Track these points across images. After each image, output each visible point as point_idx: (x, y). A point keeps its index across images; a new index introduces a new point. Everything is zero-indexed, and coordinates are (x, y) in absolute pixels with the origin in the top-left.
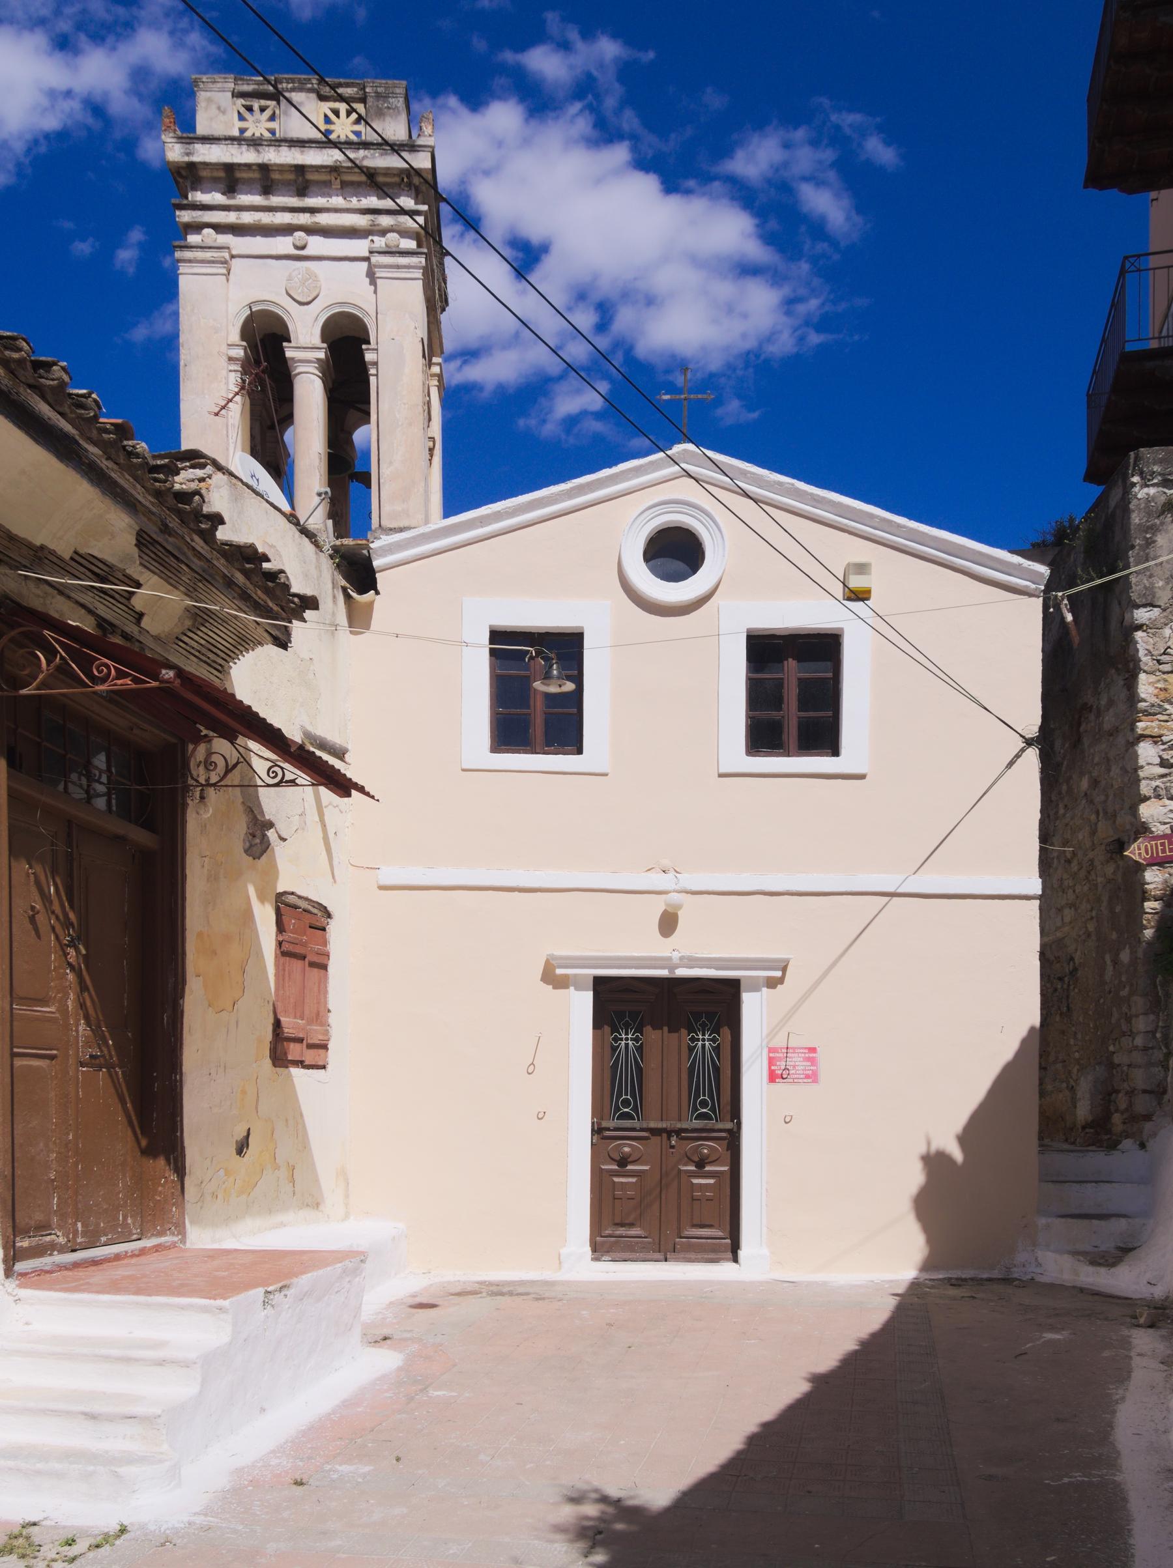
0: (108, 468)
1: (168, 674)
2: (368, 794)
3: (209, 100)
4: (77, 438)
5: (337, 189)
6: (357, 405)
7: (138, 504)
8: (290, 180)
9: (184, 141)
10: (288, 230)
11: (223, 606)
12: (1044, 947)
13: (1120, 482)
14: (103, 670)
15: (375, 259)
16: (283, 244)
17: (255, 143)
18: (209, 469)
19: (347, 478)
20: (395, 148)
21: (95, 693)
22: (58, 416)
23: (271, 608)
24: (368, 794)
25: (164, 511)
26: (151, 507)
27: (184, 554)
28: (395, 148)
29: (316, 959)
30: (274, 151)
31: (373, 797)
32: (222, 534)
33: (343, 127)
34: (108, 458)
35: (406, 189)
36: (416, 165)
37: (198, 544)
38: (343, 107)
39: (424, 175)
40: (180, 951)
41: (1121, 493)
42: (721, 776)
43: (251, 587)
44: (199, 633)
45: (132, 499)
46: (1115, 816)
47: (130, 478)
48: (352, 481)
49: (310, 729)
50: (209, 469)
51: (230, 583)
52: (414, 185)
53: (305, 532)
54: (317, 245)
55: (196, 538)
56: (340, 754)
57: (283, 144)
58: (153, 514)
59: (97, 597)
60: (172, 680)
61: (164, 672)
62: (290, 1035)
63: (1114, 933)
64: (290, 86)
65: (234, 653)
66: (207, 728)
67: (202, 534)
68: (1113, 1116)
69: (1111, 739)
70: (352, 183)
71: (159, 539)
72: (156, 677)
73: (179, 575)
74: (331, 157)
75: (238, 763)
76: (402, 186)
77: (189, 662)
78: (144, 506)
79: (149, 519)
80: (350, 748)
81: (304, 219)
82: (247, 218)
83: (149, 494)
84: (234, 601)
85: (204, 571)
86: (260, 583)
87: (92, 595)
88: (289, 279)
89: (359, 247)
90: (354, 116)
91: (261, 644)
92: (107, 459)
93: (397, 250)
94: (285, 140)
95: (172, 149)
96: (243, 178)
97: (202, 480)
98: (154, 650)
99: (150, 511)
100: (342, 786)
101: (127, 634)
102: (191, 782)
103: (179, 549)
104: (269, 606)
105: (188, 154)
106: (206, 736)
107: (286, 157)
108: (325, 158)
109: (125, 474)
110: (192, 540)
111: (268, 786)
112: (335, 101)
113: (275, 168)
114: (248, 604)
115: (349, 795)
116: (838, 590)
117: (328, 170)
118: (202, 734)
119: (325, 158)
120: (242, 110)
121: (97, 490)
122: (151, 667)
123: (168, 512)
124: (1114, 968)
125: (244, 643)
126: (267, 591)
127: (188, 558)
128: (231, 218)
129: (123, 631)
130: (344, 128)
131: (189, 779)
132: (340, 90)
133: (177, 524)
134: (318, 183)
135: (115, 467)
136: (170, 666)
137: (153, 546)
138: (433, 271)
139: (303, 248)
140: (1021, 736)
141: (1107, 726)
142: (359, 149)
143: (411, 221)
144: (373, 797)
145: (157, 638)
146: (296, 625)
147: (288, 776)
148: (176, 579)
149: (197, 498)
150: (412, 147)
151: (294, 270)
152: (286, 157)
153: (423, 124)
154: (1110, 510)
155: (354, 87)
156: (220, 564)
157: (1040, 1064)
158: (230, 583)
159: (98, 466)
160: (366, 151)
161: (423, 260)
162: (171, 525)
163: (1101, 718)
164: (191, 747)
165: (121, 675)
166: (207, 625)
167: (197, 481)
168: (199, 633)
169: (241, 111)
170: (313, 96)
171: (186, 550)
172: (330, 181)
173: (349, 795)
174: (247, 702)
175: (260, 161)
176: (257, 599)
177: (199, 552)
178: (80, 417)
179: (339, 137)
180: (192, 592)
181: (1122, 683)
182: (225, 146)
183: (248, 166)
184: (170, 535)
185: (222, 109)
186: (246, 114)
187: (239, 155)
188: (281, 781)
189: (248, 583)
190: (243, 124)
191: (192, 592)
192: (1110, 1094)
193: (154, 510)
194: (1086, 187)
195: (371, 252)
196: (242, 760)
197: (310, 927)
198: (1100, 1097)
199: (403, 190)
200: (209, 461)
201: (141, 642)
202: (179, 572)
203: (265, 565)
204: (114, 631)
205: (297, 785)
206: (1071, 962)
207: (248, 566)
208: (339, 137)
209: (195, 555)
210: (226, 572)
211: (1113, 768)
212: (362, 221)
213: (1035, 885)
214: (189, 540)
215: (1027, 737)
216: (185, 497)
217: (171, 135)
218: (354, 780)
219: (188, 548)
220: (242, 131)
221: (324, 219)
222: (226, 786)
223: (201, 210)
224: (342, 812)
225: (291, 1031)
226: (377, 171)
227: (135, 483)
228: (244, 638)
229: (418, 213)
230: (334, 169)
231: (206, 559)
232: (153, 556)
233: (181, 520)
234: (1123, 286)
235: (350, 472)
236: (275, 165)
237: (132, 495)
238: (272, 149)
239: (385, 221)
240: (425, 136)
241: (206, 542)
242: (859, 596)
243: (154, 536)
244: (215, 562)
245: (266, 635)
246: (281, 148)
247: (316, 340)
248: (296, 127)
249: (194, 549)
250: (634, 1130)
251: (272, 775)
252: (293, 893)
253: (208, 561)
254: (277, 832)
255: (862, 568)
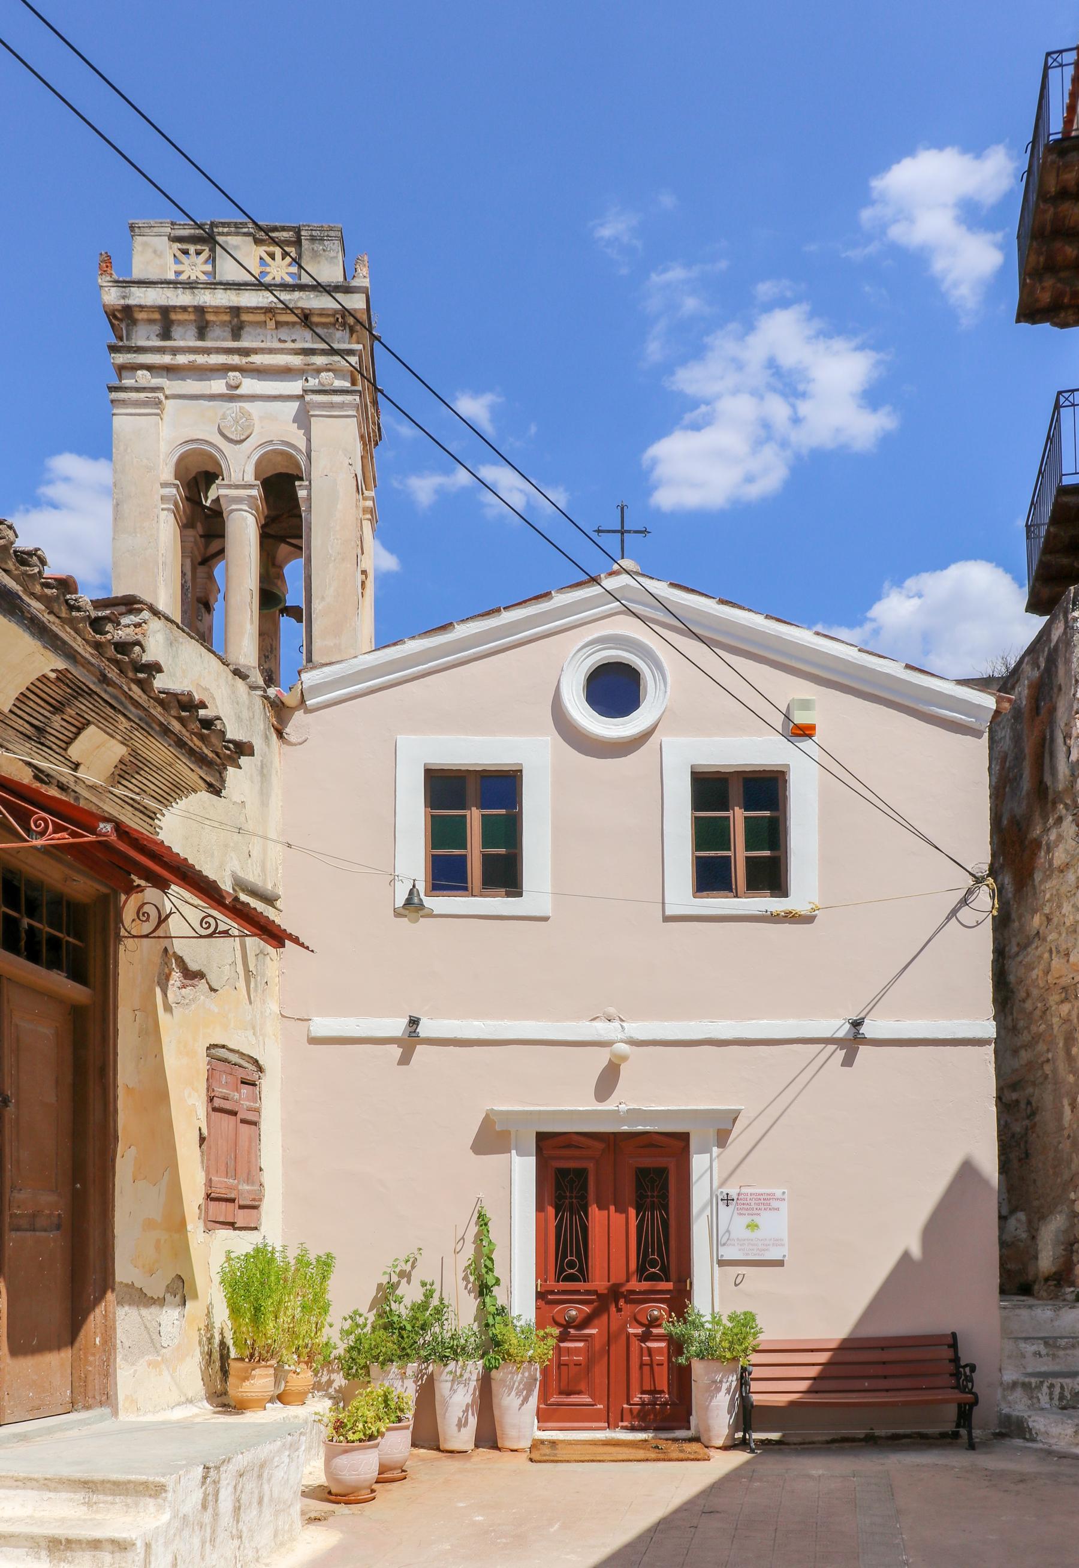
0: (49, 622)
1: (106, 828)
2: (302, 945)
3: (145, 245)
4: (21, 593)
5: (271, 329)
6: (288, 540)
7: (79, 656)
8: (225, 321)
9: (120, 285)
10: (224, 370)
11: (158, 751)
12: (1000, 1090)
13: (1061, 617)
14: (40, 824)
15: (308, 398)
16: (218, 386)
17: (191, 285)
18: (146, 614)
19: (278, 611)
20: (329, 290)
21: (34, 848)
22: (3, 573)
23: (206, 755)
24: (302, 945)
25: (103, 662)
26: (91, 658)
27: (121, 703)
28: (329, 290)
29: (250, 1116)
30: (210, 294)
31: (307, 948)
32: (160, 682)
33: (279, 269)
34: (51, 612)
35: (341, 328)
36: (348, 306)
37: (136, 692)
38: (278, 251)
39: (358, 315)
40: (111, 1109)
41: (1063, 627)
42: (667, 919)
43: (187, 734)
44: (133, 781)
45: (73, 652)
46: (1067, 955)
47: (71, 631)
48: (283, 616)
49: (241, 874)
50: (146, 614)
51: (166, 731)
52: (349, 324)
53: (237, 673)
54: (250, 385)
55: (134, 687)
56: (270, 900)
57: (219, 287)
58: (92, 665)
59: (34, 749)
60: (109, 834)
61: (102, 825)
62: (222, 1195)
63: (1071, 1076)
64: (226, 230)
65: (168, 800)
66: (140, 878)
67: (139, 683)
68: (1076, 1268)
69: (1062, 875)
70: (287, 323)
71: (98, 690)
72: (93, 831)
73: (116, 724)
74: (263, 299)
75: (171, 913)
76: (337, 326)
77: (124, 811)
78: (82, 657)
79: (88, 671)
80: (280, 891)
81: (235, 360)
82: (182, 359)
83: (90, 646)
84: (169, 748)
85: (140, 720)
86: (195, 730)
87: (30, 746)
88: (224, 417)
89: (295, 387)
90: (288, 259)
91: (195, 791)
92: (49, 613)
93: (332, 388)
94: (221, 283)
95: (109, 293)
96: (179, 320)
97: (138, 625)
98: (89, 800)
99: (89, 663)
100: (275, 936)
101: (63, 784)
102: (123, 933)
103: (115, 698)
104: (204, 753)
105: (124, 298)
106: (139, 886)
107: (222, 299)
108: (261, 299)
109: (66, 627)
110: (130, 689)
111: (201, 937)
112: (269, 245)
113: (210, 310)
114: (184, 751)
115: (283, 946)
116: (778, 721)
117: (263, 311)
118: (135, 884)
119: (261, 299)
120: (178, 254)
121: (39, 643)
122: (85, 820)
123: (107, 663)
124: (1072, 1111)
125: (177, 790)
126: (202, 738)
127: (126, 708)
128: (167, 359)
129: (58, 781)
130: (280, 270)
131: (122, 930)
132: (273, 235)
133: (115, 674)
134: (251, 323)
135: (57, 621)
136: (107, 820)
137: (91, 697)
138: (366, 406)
139: (237, 387)
140: (971, 874)
141: (1057, 863)
142: (294, 291)
143: (344, 363)
144: (307, 948)
145: (92, 787)
146: (231, 770)
147: (222, 927)
148: (112, 727)
149: (137, 649)
150: (347, 290)
151: (228, 409)
152: (222, 299)
153: (358, 266)
154: (1052, 645)
155: (291, 231)
156: (157, 712)
157: (999, 1212)
158: (166, 731)
159: (39, 620)
160: (301, 293)
161: (357, 398)
162: (109, 675)
163: (1051, 854)
164: (123, 897)
165: (58, 829)
166: (142, 772)
167: (132, 626)
168: (133, 781)
169: (177, 255)
170: (250, 239)
171: (123, 699)
172: (265, 322)
173: (283, 946)
174: (182, 855)
175: (196, 304)
176: (192, 745)
177: (137, 702)
178: (25, 573)
179: (274, 278)
180: (128, 741)
181: (1070, 818)
182: (161, 290)
183: (184, 309)
184: (108, 685)
185: (158, 252)
186: (183, 257)
187: (175, 298)
188: (214, 932)
189: (184, 731)
190: (180, 268)
191: (128, 741)
192: (1072, 1245)
193: (93, 661)
194: (1018, 321)
195: (305, 391)
196: (174, 910)
197: (242, 1082)
198: (1062, 1247)
199: (338, 329)
200: (145, 607)
201: (76, 792)
202: (117, 722)
203: (202, 712)
204: (50, 782)
205: (231, 936)
206: (1029, 1106)
207: (183, 714)
208: (274, 278)
209: (133, 704)
210: (162, 720)
211: (1065, 905)
212: (296, 361)
213: (988, 1029)
214: (127, 690)
215: (977, 875)
216: (123, 647)
217: (109, 278)
218: (289, 931)
219: (126, 697)
220: (178, 273)
221: (257, 359)
222: (159, 937)
223: (135, 352)
224: (272, 960)
225: (218, 1190)
226: (312, 312)
227: (76, 635)
228: (178, 786)
229: (351, 352)
230: (269, 310)
231: (143, 707)
232: (91, 706)
233: (120, 670)
234: (1058, 420)
235: (281, 606)
236: (210, 307)
237: (72, 647)
238: (207, 292)
239: (320, 360)
240: (359, 277)
241: (143, 690)
242: (805, 732)
243: (92, 687)
244: (152, 711)
245: (200, 782)
246: (216, 291)
247: (250, 477)
248: (229, 270)
249: (131, 698)
250: (577, 1292)
251: (205, 926)
252: (223, 1047)
253: (145, 709)
254: (208, 983)
255: (806, 705)
